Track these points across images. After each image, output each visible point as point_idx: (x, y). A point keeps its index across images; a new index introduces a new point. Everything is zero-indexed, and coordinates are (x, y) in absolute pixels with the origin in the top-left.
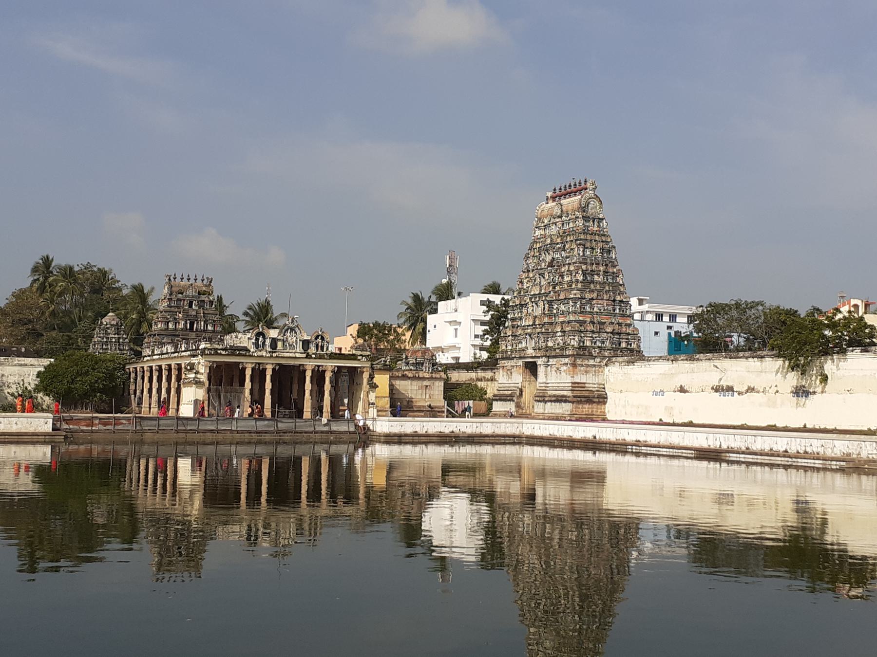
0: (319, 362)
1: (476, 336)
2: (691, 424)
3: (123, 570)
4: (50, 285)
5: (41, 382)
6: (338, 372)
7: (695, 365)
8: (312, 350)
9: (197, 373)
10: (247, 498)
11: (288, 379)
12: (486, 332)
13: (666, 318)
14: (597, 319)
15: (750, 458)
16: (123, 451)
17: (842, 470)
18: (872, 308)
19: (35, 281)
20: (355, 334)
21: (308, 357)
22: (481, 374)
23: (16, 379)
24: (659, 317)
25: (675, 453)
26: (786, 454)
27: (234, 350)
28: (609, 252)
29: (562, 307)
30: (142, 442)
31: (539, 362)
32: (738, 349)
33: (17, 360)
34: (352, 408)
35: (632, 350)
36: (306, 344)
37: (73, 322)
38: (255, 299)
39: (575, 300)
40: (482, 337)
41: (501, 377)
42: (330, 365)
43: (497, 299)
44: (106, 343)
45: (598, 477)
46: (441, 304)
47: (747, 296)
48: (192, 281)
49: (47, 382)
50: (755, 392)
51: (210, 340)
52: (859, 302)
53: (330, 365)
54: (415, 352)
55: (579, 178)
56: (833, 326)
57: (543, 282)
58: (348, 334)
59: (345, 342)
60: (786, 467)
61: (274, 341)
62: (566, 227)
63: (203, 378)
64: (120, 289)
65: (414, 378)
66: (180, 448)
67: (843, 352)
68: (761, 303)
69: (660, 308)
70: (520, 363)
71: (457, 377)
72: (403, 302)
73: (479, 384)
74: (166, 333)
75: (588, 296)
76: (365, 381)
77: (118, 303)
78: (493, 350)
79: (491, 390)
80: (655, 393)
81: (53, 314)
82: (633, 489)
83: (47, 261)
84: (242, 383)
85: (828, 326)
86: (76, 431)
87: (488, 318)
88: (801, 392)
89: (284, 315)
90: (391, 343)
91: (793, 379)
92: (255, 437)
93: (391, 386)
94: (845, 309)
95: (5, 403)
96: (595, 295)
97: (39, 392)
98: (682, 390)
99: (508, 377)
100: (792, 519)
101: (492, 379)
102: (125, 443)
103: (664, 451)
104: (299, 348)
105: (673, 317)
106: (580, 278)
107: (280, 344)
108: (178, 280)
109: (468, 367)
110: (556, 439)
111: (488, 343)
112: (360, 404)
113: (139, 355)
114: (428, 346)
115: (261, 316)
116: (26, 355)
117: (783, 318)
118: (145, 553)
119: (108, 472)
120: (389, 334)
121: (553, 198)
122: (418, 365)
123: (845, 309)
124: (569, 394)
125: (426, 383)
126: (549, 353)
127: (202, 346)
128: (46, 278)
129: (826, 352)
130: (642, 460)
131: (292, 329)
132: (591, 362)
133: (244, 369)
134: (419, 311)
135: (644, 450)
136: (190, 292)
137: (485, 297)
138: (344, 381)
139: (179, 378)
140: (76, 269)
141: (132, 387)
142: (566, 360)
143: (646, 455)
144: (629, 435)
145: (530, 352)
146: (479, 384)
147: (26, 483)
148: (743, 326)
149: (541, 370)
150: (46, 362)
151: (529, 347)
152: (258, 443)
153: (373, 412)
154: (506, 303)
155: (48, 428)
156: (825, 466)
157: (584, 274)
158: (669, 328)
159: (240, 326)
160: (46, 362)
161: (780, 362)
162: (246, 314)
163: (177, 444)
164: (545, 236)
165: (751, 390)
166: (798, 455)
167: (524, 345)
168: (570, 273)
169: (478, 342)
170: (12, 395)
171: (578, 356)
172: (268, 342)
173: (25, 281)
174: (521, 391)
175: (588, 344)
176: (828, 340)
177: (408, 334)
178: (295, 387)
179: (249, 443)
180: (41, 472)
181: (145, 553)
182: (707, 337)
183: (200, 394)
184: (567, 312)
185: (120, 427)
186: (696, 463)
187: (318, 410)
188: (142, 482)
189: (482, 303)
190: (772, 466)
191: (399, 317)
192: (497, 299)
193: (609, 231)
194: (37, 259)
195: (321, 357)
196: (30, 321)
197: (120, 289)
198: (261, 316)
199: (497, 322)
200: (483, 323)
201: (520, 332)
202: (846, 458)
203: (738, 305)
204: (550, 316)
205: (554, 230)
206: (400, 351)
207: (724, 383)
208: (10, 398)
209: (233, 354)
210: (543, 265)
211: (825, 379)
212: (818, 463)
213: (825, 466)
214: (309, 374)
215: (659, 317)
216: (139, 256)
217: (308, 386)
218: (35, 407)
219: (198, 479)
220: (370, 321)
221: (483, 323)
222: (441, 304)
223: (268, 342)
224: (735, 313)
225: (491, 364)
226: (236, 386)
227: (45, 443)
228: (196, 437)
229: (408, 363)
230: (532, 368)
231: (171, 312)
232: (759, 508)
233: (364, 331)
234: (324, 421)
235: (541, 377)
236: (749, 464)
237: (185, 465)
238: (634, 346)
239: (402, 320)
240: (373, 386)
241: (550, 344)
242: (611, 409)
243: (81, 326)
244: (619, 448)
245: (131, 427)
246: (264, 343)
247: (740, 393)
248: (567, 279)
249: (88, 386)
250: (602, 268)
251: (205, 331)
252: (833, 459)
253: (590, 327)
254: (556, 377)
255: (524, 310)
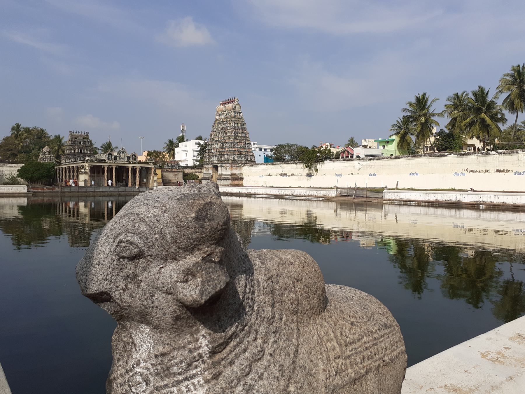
0: (134, 165)
1: (194, 156)
2: (272, 187)
3: (58, 246)
4: (20, 135)
5: (20, 173)
6: (141, 169)
7: (274, 166)
8: (131, 160)
9: (85, 169)
10: (107, 215)
11: (121, 171)
12: (198, 155)
13: (263, 150)
14: (240, 150)
15: (293, 198)
16: (56, 200)
17: (323, 201)
18: (333, 146)
19: (13, 133)
20: (146, 155)
21: (130, 163)
22: (197, 170)
23: (8, 172)
24: (261, 149)
25: (268, 197)
26: (305, 196)
27: (100, 161)
28: (243, 125)
29: (227, 145)
30: (64, 196)
31: (219, 165)
32: (288, 161)
33: (8, 165)
34: (148, 181)
35: (252, 161)
36: (128, 158)
37: (30, 150)
38: (104, 141)
39: (231, 143)
40: (196, 156)
41: (204, 171)
42: (138, 166)
43: (202, 142)
44: (45, 158)
45: (241, 206)
46: (180, 144)
47: (291, 142)
48: (80, 134)
49: (22, 173)
50: (293, 176)
51: (89, 156)
52: (328, 144)
53: (138, 166)
54: (171, 162)
55: (232, 97)
56: (320, 152)
57: (220, 136)
58: (143, 155)
59: (142, 158)
60: (305, 200)
61: (116, 157)
62: (228, 115)
63: (88, 171)
64: (49, 137)
65: (171, 171)
66: (80, 198)
67: (323, 161)
68: (296, 145)
69: (261, 146)
70: (212, 166)
71: (187, 171)
72: (165, 143)
73: (196, 174)
74: (70, 154)
75: (236, 141)
76: (152, 172)
77: (49, 143)
78: (201, 161)
79: (201, 176)
80: (260, 176)
81: (22, 147)
82: (252, 210)
83: (18, 126)
84: (103, 173)
85: (318, 152)
86: (37, 192)
87: (199, 149)
88: (309, 175)
89: (117, 148)
90: (161, 158)
91: (306, 171)
92: (110, 194)
93: (162, 174)
94: (324, 146)
95: (4, 182)
96: (238, 141)
97: (19, 177)
98: (269, 175)
99: (207, 171)
100: (306, 218)
101: (201, 172)
102: (58, 197)
103: (264, 196)
104: (126, 159)
105: (265, 150)
106: (233, 135)
107: (118, 158)
108: (75, 133)
109: (191, 167)
110: (226, 193)
111: (199, 159)
112: (151, 181)
113: (60, 163)
114: (177, 158)
115: (108, 148)
116: (12, 163)
117: (303, 150)
118: (65, 238)
119: (49, 209)
120: (160, 155)
121: (223, 104)
122: (172, 166)
123: (324, 146)
124: (230, 177)
125: (176, 173)
126: (222, 162)
127: (87, 159)
128: (18, 132)
129: (318, 161)
130: (256, 199)
131: (123, 152)
132: (238, 165)
133: (104, 168)
134: (171, 147)
135: (257, 196)
136: (80, 138)
137: (197, 141)
138: (144, 172)
139: (77, 172)
140: (31, 129)
141: (58, 175)
142: (229, 165)
143: (258, 198)
144: (252, 191)
145: (215, 162)
146: (196, 174)
147: (15, 213)
148: (290, 152)
149: (219, 169)
150: (21, 165)
151: (215, 160)
152: (111, 196)
153: (156, 184)
154: (206, 144)
155: (25, 191)
156: (318, 199)
157: (235, 133)
158: (264, 153)
159: (100, 152)
160: (21, 165)
161: (302, 165)
162: (102, 147)
163: (78, 197)
164: (220, 119)
165: (292, 175)
166: (309, 196)
167: (213, 159)
168: (229, 132)
169: (195, 158)
170: (7, 179)
171: (233, 163)
172: (113, 157)
173: (8, 133)
174: (212, 176)
175: (236, 159)
176: (318, 157)
177: (168, 155)
178: (125, 175)
179: (107, 196)
180: (21, 208)
181: (65, 238)
182: (277, 157)
183: (86, 177)
184: (229, 147)
185: (55, 190)
186: (275, 200)
187: (134, 183)
188: (64, 211)
189: (196, 144)
190: (300, 200)
191: (164, 148)
192: (202, 142)
193: (243, 117)
194: (14, 124)
195: (135, 163)
196: (12, 150)
197: (49, 137)
198: (108, 148)
199: (202, 151)
200: (197, 151)
201: (211, 154)
202: (324, 197)
203: (288, 145)
204: (222, 148)
205: (223, 116)
206: (165, 162)
207: (284, 173)
208: (6, 180)
209: (99, 162)
210: (219, 129)
211: (317, 170)
212: (315, 199)
213: (318, 199)
214: (130, 170)
215: (261, 149)
216: (58, 125)
217: (130, 174)
218: (19, 184)
219: (87, 210)
220: (152, 150)
221: (197, 151)
222: (180, 144)
223: (113, 157)
224: (287, 148)
225: (201, 166)
226: (101, 174)
227: (24, 197)
228: (86, 194)
229: (168, 166)
230: (216, 168)
231: (73, 145)
232: (295, 214)
233: (150, 154)
234: (137, 187)
235: (220, 171)
236: (293, 200)
237: (82, 205)
238: (253, 160)
239: (165, 150)
240: (156, 174)
241: (223, 159)
242: (245, 182)
243: (34, 151)
244: (248, 195)
245: (60, 190)
246: (111, 158)
247: (289, 176)
248: (228, 135)
249: (38, 175)
250: (241, 131)
251: (87, 153)
252: (320, 197)
253: (237, 153)
254: (225, 171)
255: (213, 146)
